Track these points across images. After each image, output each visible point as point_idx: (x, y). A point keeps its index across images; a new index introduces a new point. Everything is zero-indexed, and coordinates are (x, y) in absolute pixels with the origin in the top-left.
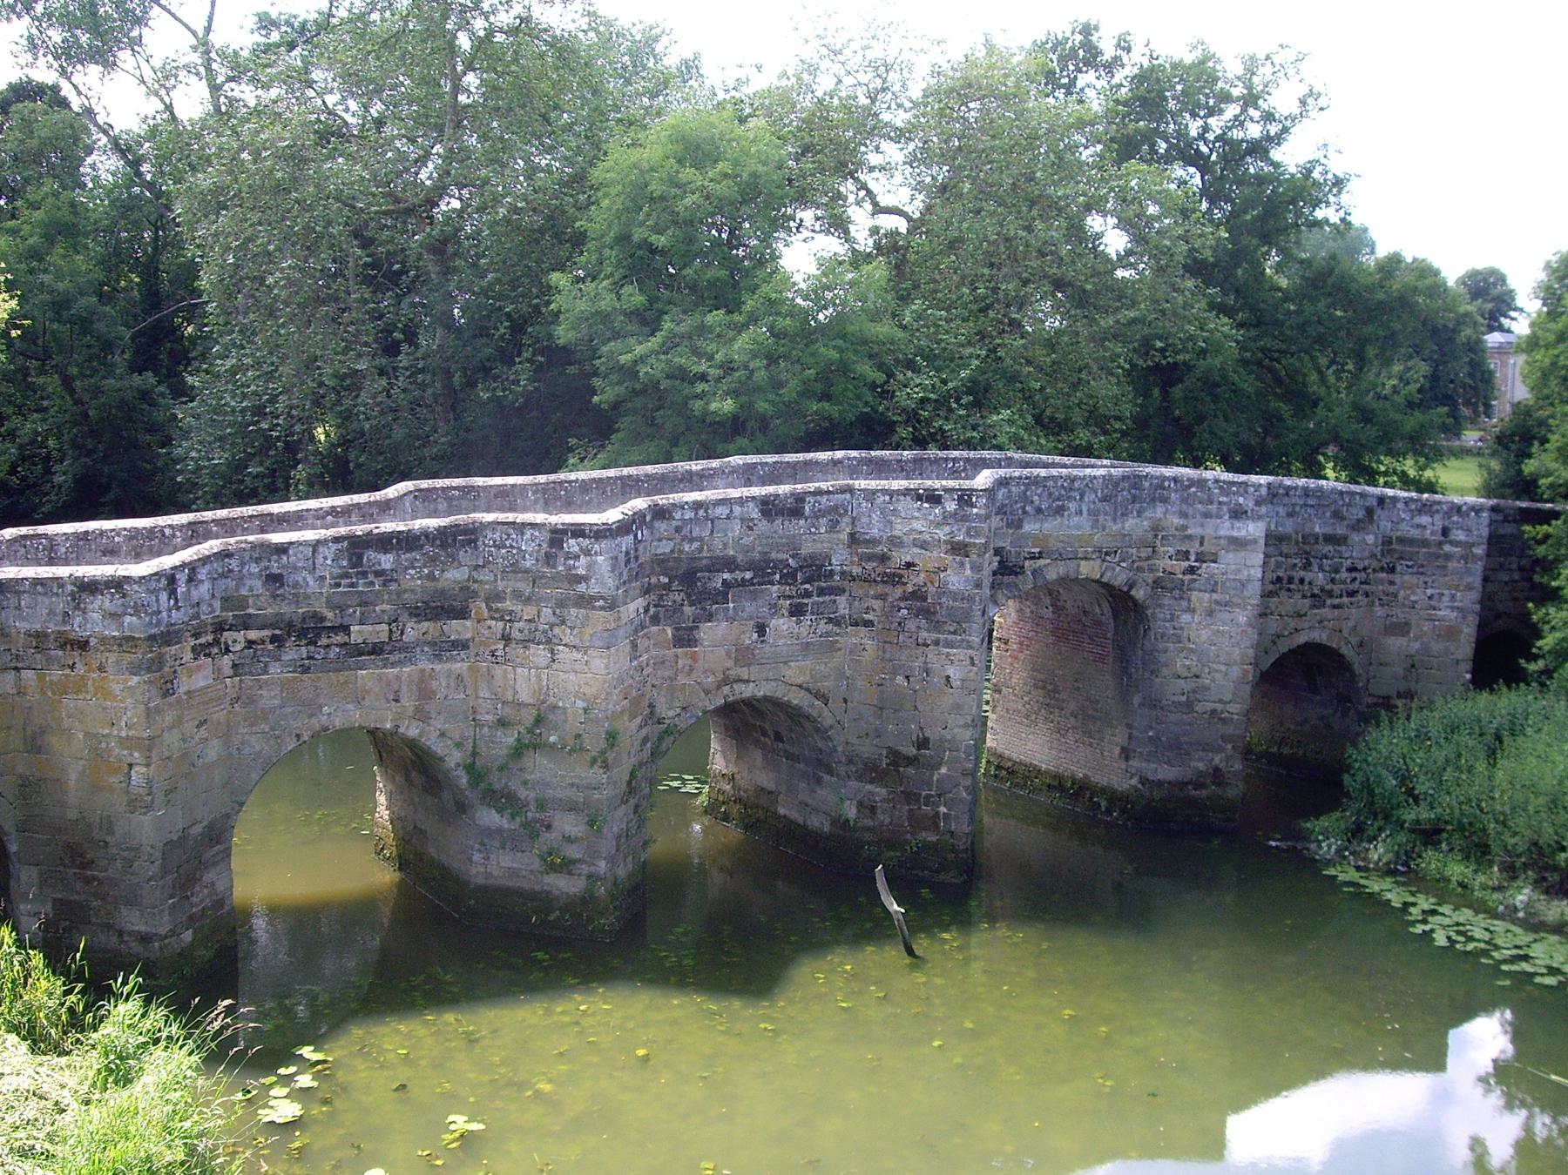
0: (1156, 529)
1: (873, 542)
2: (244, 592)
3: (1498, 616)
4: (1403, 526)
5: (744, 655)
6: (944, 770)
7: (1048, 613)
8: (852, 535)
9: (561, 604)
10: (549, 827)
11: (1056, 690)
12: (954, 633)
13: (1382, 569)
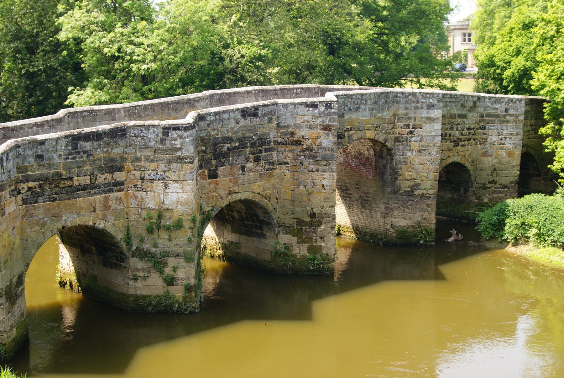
0: (395, 115)
1: (287, 127)
2: (26, 164)
8: (278, 124)
9: (169, 162)
12: (326, 165)
13: (480, 128)
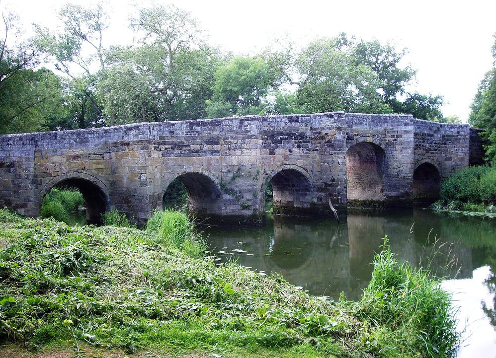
0: (385, 130)
1: (317, 129)
3: (474, 158)
4: (447, 132)
5: (286, 158)
6: (339, 187)
7: (357, 158)
8: (311, 128)
9: (244, 138)
10: (243, 197)
11: (361, 178)
13: (443, 144)
